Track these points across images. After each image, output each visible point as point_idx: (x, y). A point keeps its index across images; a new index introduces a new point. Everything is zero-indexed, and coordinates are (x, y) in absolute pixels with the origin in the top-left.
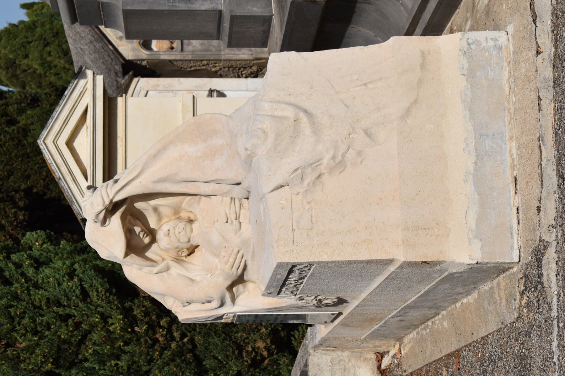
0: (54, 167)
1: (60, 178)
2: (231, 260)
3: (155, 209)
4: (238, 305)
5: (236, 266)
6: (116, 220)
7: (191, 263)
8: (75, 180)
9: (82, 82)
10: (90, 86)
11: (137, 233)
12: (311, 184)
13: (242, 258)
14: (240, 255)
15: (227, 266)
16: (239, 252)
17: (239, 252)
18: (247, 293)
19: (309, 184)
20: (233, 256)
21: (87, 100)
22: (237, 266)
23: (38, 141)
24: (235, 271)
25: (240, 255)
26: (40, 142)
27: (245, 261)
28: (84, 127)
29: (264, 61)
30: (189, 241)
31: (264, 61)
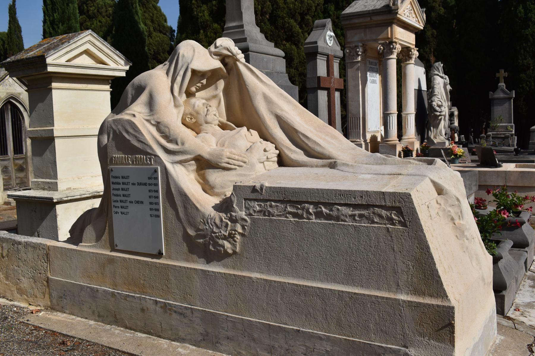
0: (76, 39)
1: (69, 42)
2: (237, 157)
3: (215, 97)
4: (174, 167)
5: (231, 161)
6: (216, 64)
7: (391, 114)
8: (67, 53)
9: (122, 62)
10: (120, 67)
11: (202, 81)
12: (450, 214)
13: (238, 166)
14: (242, 164)
15: (228, 154)
16: (245, 162)
17: (245, 162)
18: (187, 173)
19: (450, 211)
20: (240, 158)
21: (113, 65)
22: (231, 162)
23: (90, 30)
24: (225, 161)
25: (242, 164)
26: (90, 31)
27: (235, 169)
28: (95, 63)
29: (52, 174)
30: (207, 123)
31: (52, 174)
